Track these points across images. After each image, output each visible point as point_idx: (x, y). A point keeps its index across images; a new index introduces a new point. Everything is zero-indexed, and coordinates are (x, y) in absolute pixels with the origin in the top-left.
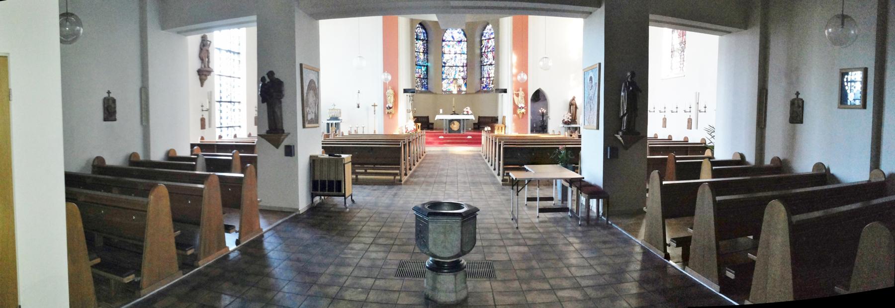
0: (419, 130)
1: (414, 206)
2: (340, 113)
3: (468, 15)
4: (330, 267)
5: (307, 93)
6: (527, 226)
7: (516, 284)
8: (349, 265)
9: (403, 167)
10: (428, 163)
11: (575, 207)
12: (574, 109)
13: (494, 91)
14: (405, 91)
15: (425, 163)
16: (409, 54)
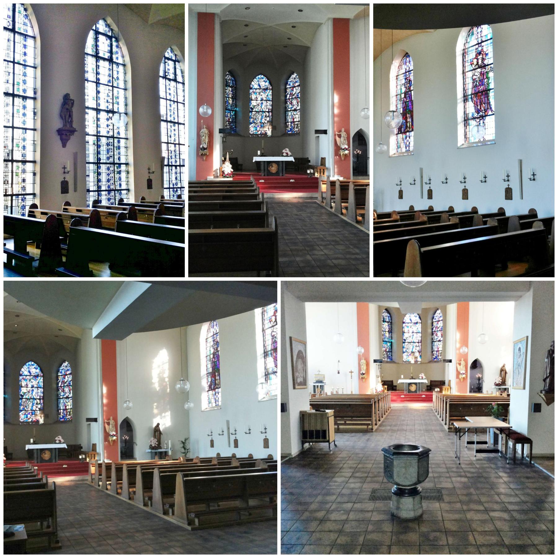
0: (386, 391)
1: (382, 448)
2: (324, 377)
3: (423, 303)
4: (318, 497)
5: (297, 361)
6: (467, 462)
7: (458, 506)
8: (333, 494)
9: (374, 419)
10: (393, 416)
11: (504, 450)
12: (504, 374)
13: (442, 361)
14: (375, 361)
15: (391, 415)
16: (377, 333)
